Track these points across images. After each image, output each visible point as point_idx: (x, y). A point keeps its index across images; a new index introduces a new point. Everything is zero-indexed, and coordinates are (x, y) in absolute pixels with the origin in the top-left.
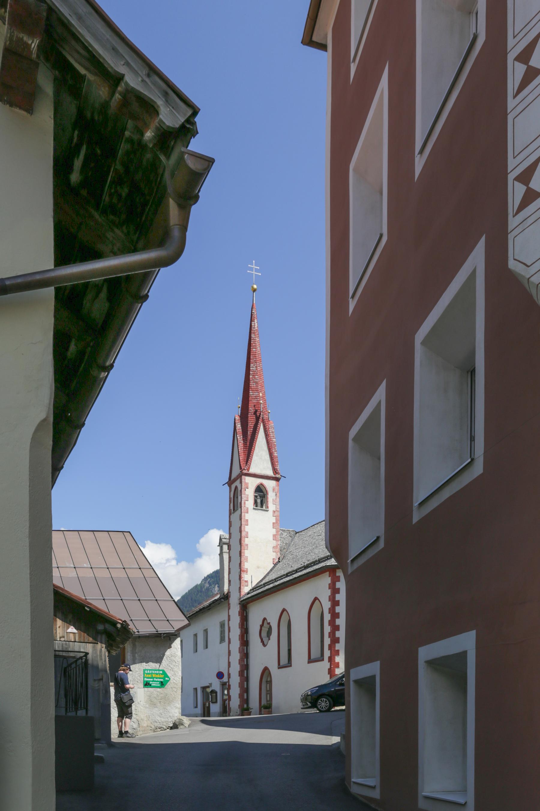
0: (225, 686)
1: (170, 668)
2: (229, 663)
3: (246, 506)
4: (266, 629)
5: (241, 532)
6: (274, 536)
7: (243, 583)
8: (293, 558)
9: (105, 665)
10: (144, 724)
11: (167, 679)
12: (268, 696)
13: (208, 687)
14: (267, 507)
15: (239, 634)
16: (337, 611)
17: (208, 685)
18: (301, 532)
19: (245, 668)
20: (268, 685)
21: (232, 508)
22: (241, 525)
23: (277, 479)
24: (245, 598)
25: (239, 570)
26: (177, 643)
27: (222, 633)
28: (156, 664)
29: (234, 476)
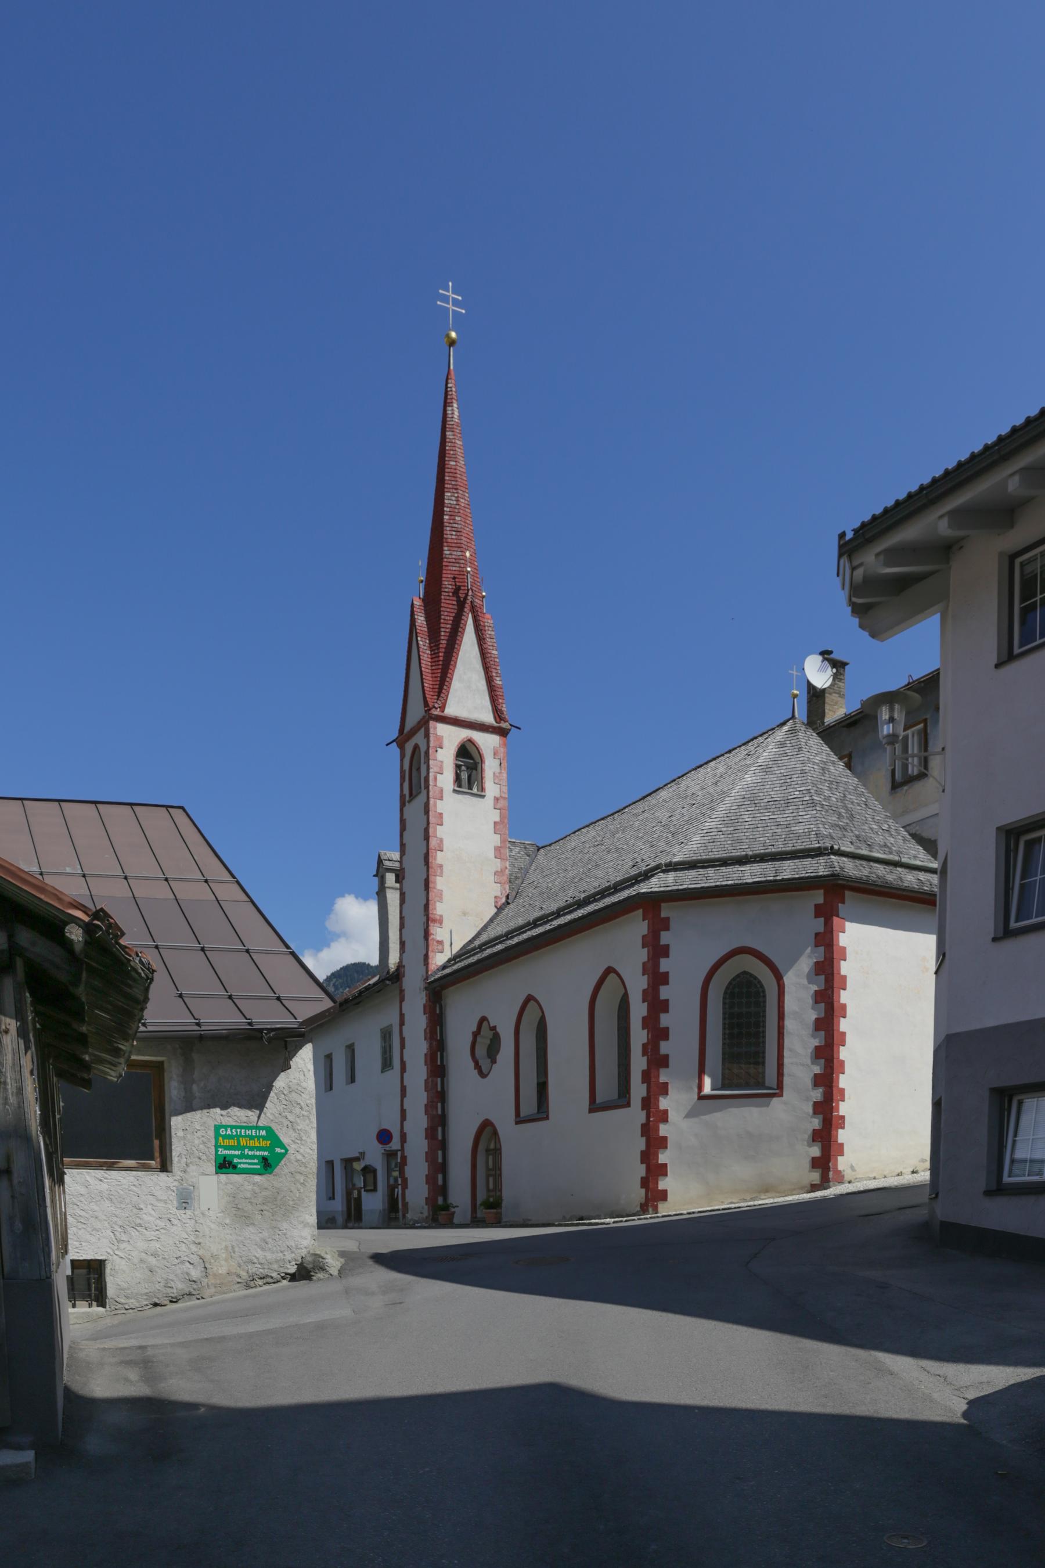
0: (396, 1160)
1: (286, 1123)
2: (403, 1112)
4: (486, 1044)
5: (427, 838)
6: (497, 849)
7: (433, 946)
8: (541, 893)
9: (21, 1106)
11: (278, 1150)
12: (491, 1179)
13: (357, 1159)
14: (483, 789)
15: (425, 1051)
16: (662, 997)
17: (358, 1155)
18: (550, 845)
20: (491, 1158)
21: (406, 791)
22: (428, 823)
23: (503, 733)
24: (437, 977)
25: (424, 919)
26: (305, 1058)
28: (249, 1113)
29: (409, 724)
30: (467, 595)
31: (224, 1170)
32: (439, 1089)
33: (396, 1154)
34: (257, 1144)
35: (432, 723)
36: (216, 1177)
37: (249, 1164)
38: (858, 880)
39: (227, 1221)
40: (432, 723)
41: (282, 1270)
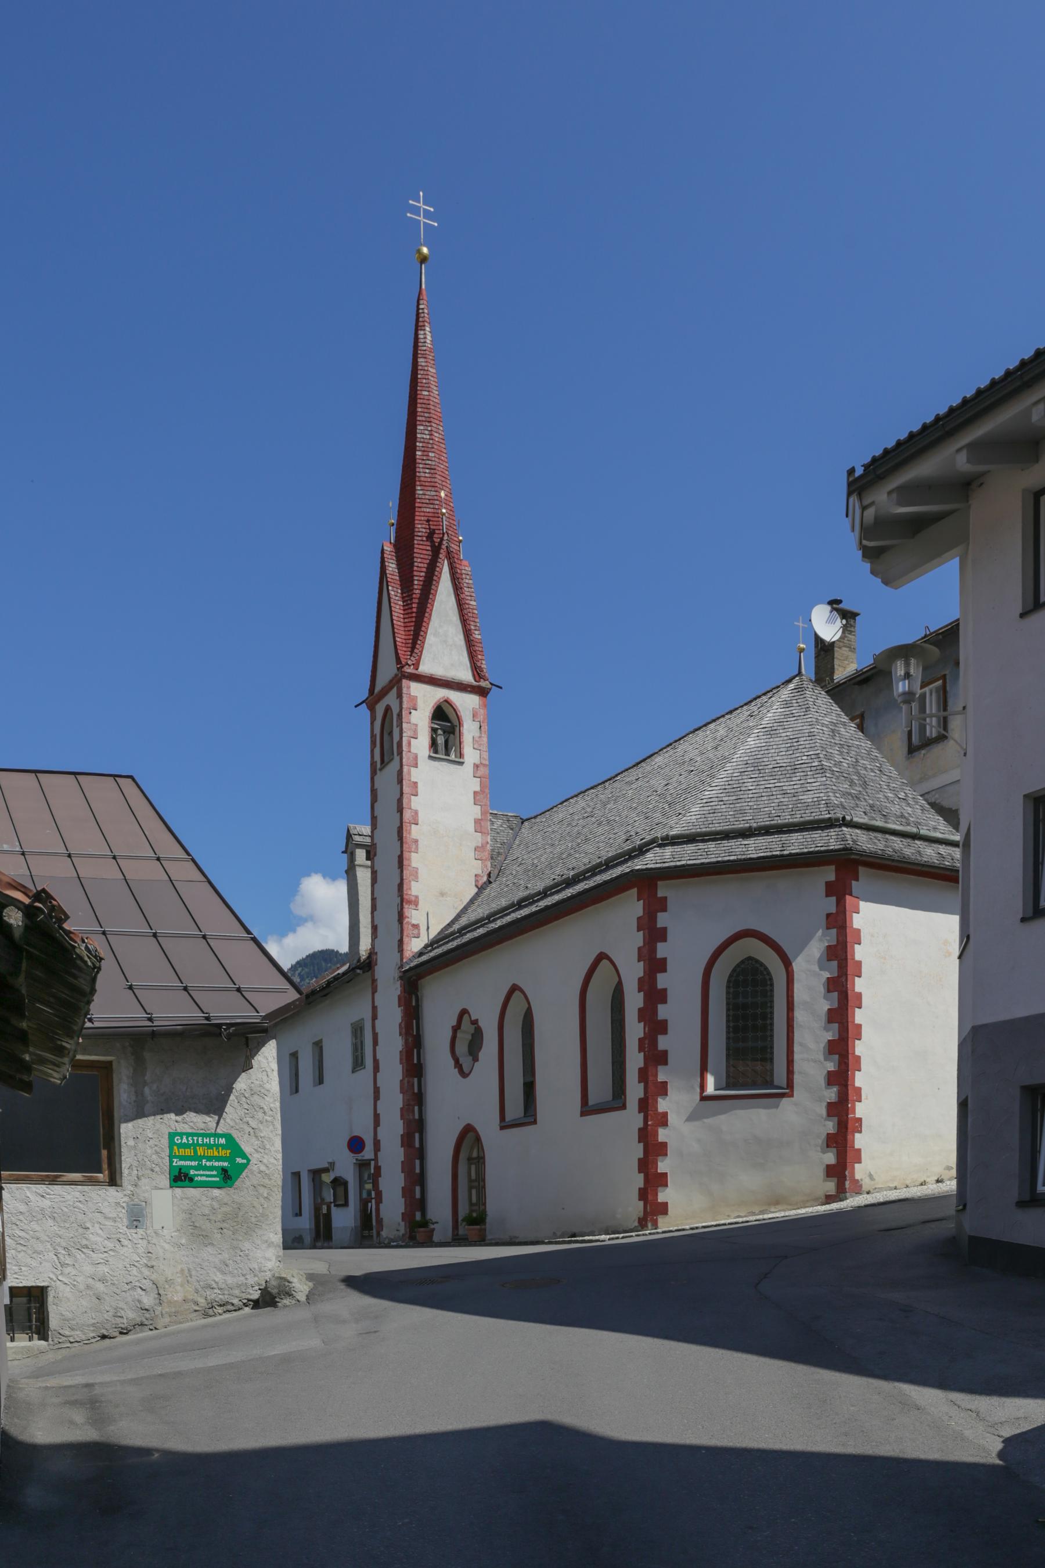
1: (248, 1129)
3: (413, 750)
5: (400, 810)
6: (477, 822)
7: (408, 930)
8: (526, 871)
10: (176, 1294)
11: (239, 1160)
12: (474, 1192)
13: (326, 1170)
14: (461, 755)
16: (660, 986)
17: (327, 1165)
18: (535, 817)
19: (415, 1129)
20: (473, 1167)
21: (377, 758)
23: (482, 692)
24: (412, 965)
25: (398, 900)
27: (358, 1049)
28: (207, 1119)
29: (381, 683)
30: (442, 539)
31: (179, 1183)
32: (416, 1090)
33: (369, 1164)
34: (216, 1154)
35: (405, 682)
36: (170, 1191)
37: (207, 1176)
39: (183, 1241)
40: (405, 682)
41: (244, 1296)
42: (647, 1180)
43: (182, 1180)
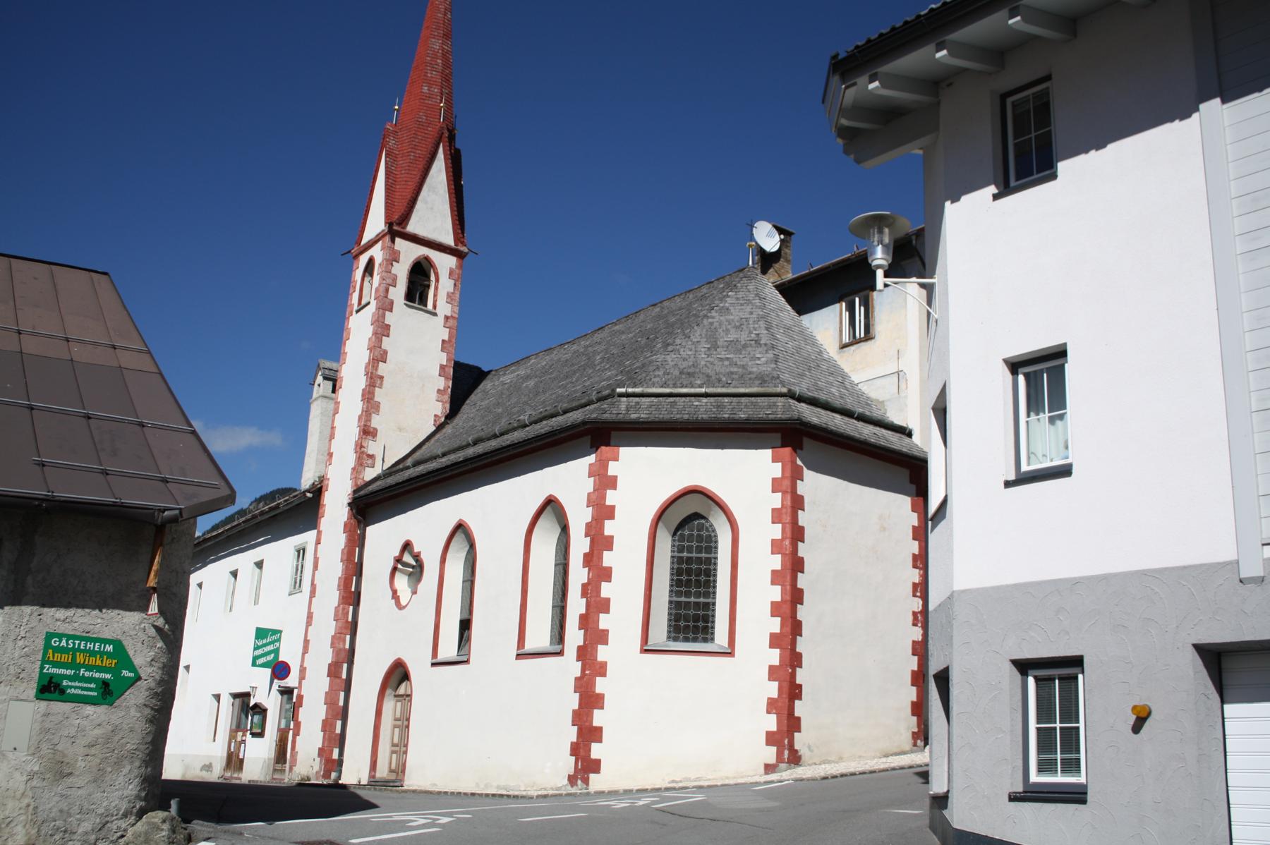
2: (306, 642)
4: (409, 563)
11: (125, 673)
16: (607, 533)
19: (344, 659)
31: (47, 695)
34: (99, 662)
37: (83, 689)
38: (814, 427)
42: (580, 733)
43: (50, 692)
